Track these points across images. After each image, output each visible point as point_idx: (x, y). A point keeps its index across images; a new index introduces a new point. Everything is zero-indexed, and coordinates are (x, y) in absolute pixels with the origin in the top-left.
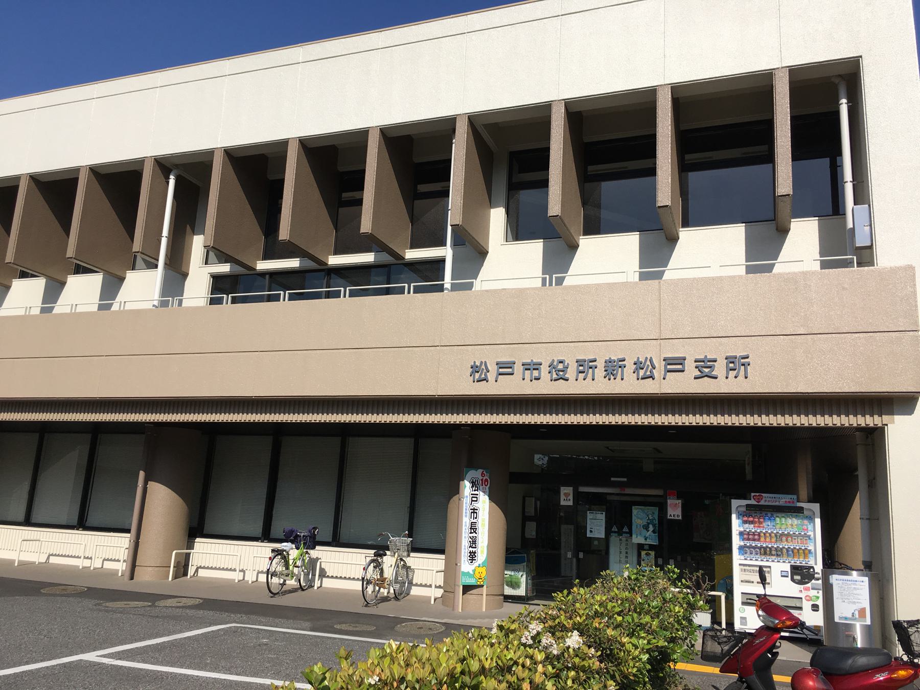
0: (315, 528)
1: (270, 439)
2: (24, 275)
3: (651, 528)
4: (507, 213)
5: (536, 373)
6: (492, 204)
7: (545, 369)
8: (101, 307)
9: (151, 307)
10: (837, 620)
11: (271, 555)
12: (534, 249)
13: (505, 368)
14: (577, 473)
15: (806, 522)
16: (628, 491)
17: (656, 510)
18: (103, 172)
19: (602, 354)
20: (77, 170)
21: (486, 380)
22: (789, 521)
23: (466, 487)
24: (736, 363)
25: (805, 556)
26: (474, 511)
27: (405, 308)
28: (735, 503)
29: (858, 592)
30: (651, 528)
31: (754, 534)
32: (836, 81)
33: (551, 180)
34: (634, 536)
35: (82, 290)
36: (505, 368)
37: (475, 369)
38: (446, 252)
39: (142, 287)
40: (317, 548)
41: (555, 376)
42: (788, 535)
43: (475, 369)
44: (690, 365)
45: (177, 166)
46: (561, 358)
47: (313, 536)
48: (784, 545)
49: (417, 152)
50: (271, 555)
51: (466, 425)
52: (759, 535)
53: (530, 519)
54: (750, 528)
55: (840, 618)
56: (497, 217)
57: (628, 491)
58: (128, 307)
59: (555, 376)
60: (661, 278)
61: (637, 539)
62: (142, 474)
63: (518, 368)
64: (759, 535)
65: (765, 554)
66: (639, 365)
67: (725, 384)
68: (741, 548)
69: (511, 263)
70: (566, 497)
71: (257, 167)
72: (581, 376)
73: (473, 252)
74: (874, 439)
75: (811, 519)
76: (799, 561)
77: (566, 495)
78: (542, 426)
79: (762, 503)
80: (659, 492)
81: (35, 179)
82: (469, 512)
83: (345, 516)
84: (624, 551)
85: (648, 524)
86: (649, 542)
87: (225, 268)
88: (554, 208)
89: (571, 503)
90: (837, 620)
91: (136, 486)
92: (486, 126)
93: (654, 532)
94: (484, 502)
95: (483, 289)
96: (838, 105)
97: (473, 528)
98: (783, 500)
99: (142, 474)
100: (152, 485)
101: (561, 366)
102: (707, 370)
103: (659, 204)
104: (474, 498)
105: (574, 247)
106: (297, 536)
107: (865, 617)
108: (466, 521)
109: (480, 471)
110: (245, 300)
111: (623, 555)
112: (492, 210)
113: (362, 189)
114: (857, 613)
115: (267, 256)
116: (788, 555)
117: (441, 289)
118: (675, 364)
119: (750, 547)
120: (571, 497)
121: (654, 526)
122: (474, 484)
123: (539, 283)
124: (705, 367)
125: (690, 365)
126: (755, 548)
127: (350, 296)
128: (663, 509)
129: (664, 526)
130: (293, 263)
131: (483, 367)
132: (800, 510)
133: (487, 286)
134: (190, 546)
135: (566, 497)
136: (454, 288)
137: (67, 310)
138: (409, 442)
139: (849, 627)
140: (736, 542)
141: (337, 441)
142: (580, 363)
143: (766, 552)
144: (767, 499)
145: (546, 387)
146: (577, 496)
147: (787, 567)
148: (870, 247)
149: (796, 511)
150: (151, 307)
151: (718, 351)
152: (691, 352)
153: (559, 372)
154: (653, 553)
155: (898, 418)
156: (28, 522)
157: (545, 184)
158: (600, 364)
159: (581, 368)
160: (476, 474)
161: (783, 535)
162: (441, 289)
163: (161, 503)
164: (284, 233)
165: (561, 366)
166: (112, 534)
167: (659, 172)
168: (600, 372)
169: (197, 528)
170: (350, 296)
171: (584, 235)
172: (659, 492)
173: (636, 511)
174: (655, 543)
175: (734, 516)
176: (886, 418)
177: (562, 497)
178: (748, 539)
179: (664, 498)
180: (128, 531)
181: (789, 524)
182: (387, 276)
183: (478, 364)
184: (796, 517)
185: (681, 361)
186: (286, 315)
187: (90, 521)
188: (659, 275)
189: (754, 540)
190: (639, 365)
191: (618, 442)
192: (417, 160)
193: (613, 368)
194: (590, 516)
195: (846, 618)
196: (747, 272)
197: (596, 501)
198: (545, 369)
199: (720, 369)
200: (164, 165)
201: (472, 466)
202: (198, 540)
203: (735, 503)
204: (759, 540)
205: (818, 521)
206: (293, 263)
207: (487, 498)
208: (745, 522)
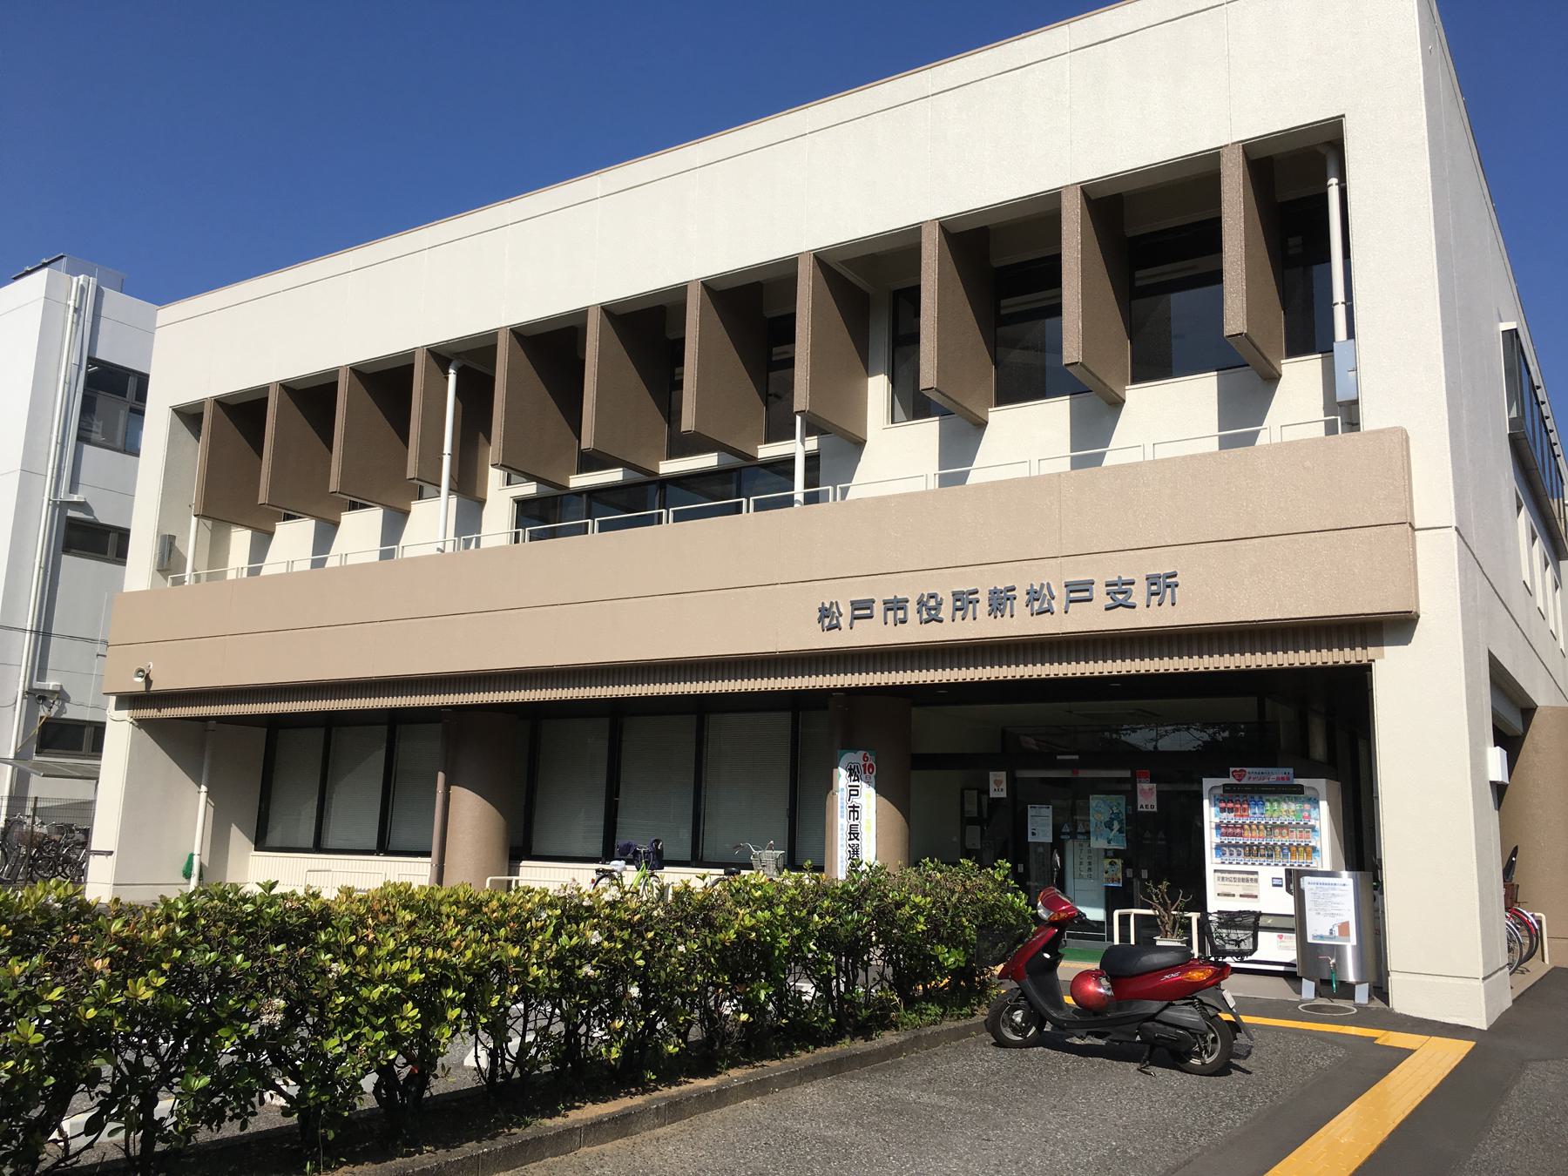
0: (657, 841)
1: (605, 722)
2: (354, 506)
3: (1116, 826)
4: (893, 380)
5: (900, 614)
6: (869, 372)
7: (912, 607)
8: (945, 481)
9: (435, 552)
10: (1310, 940)
11: (595, 877)
12: (929, 429)
13: (862, 609)
14: (1008, 754)
15: (1307, 806)
16: (1083, 774)
17: (1122, 800)
18: (369, 371)
19: (984, 582)
20: (334, 372)
21: (837, 626)
22: (1284, 806)
23: (842, 778)
24: (1162, 585)
25: (1309, 856)
26: (854, 809)
27: (747, 531)
28: (1208, 783)
29: (1337, 900)
30: (1116, 826)
31: (1235, 826)
32: (1323, 150)
33: (1226, 266)
34: (1093, 839)
35: (360, 531)
36: (862, 609)
37: (825, 613)
38: (798, 448)
39: (431, 519)
40: (666, 869)
41: (925, 616)
42: (1282, 826)
43: (825, 613)
44: (1099, 591)
45: (458, 355)
46: (932, 591)
47: (659, 853)
48: (1278, 840)
49: (753, 307)
50: (595, 877)
51: (843, 689)
52: (1242, 827)
53: (972, 821)
54: (1230, 817)
55: (1315, 937)
56: (878, 388)
57: (1083, 774)
58: (351, 561)
59: (925, 616)
60: (1253, 444)
61: (1098, 843)
62: (441, 776)
63: (878, 608)
64: (1242, 827)
65: (1250, 854)
66: (1034, 596)
67: (1145, 616)
68: (1219, 847)
69: (898, 451)
70: (998, 785)
71: (552, 346)
72: (1155, 599)
73: (843, 446)
74: (1359, 680)
75: (1314, 802)
76: (1297, 863)
77: (998, 783)
78: (940, 685)
79: (1245, 781)
80: (1127, 774)
81: (287, 387)
82: (846, 811)
83: (708, 828)
84: (1086, 861)
85: (1112, 820)
86: (1113, 846)
87: (530, 489)
88: (1235, 320)
89: (1003, 794)
90: (1310, 940)
91: (435, 793)
92: (847, 263)
93: (1120, 831)
94: (868, 796)
95: (1286, 439)
96: (1326, 187)
97: (854, 833)
98: (1274, 775)
99: (441, 776)
100: (455, 790)
101: (932, 603)
102: (1120, 597)
103: (1066, 361)
104: (854, 792)
105: (1117, 404)
106: (636, 853)
107: (1348, 934)
108: (842, 823)
109: (861, 753)
110: (553, 534)
111: (1085, 866)
112: (871, 380)
113: (793, 341)
114: (1336, 929)
115: (672, 455)
116: (1285, 856)
117: (789, 502)
118: (1079, 591)
119: (1229, 845)
120: (1004, 786)
121: (1120, 822)
122: (852, 772)
123: (1319, 430)
124: (1120, 593)
125: (1099, 591)
126: (1236, 845)
127: (756, 510)
128: (1132, 798)
129: (1135, 823)
130: (709, 461)
131: (1045, 591)
132: (1300, 790)
133: (409, 553)
134: (514, 871)
135: (998, 785)
136: (811, 499)
137: (282, 569)
138: (784, 718)
139: (1337, 951)
140: (1211, 838)
141: (692, 720)
142: (957, 596)
143: (1252, 851)
144: (1252, 775)
145: (914, 633)
146: (1012, 782)
147: (1280, 872)
148: (1356, 402)
149: (1294, 792)
150: (435, 552)
151: (1137, 569)
152: (1100, 573)
153: (930, 610)
154: (1119, 862)
155: (1388, 650)
156: (318, 847)
157: (1216, 277)
158: (983, 597)
159: (1154, 588)
160: (856, 757)
161: (1274, 826)
162: (789, 502)
163: (469, 816)
164: (688, 422)
165: (932, 603)
166: (419, 859)
167: (1227, 277)
168: (983, 607)
169: (519, 849)
170: (756, 510)
171: (1134, 381)
172: (1127, 774)
173: (1095, 802)
174: (1122, 846)
175: (1206, 803)
176: (1372, 652)
177: (992, 786)
178: (1227, 835)
179: (1133, 781)
180: (428, 854)
181: (1285, 811)
182: (739, 484)
183: (1037, 587)
184: (1296, 800)
185: (1087, 586)
186: (597, 552)
187: (330, 841)
188: (1251, 439)
189: (1234, 835)
190: (1034, 596)
191: (1065, 705)
192: (997, 262)
193: (1000, 601)
194: (1031, 812)
195: (1322, 937)
196: (1073, 468)
197: (1044, 792)
198: (912, 607)
199: (1139, 594)
200: (440, 356)
201: (850, 746)
202: (524, 863)
203: (1208, 783)
204: (1241, 835)
205: (1324, 805)
206: (709, 461)
207: (872, 791)
208: (1223, 810)
